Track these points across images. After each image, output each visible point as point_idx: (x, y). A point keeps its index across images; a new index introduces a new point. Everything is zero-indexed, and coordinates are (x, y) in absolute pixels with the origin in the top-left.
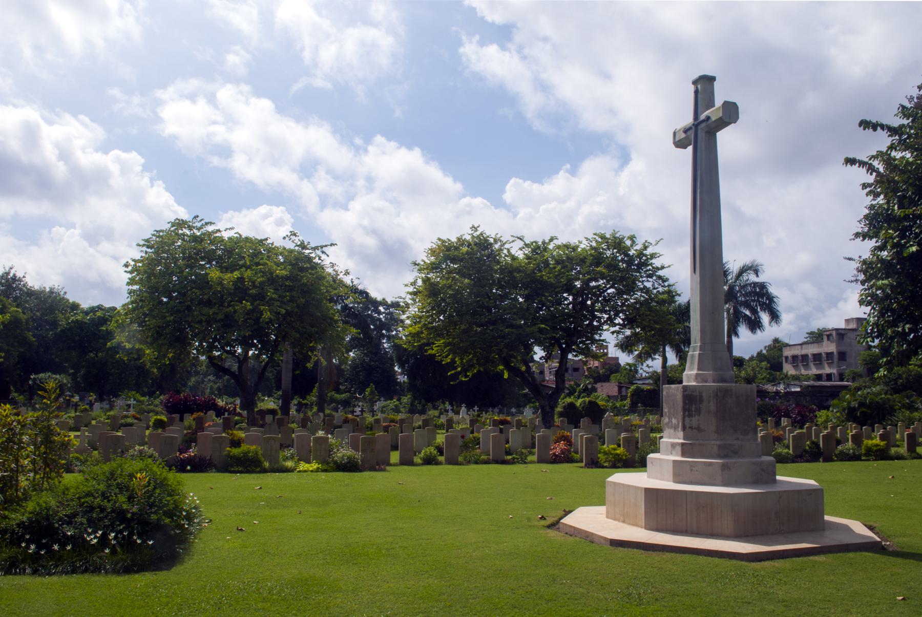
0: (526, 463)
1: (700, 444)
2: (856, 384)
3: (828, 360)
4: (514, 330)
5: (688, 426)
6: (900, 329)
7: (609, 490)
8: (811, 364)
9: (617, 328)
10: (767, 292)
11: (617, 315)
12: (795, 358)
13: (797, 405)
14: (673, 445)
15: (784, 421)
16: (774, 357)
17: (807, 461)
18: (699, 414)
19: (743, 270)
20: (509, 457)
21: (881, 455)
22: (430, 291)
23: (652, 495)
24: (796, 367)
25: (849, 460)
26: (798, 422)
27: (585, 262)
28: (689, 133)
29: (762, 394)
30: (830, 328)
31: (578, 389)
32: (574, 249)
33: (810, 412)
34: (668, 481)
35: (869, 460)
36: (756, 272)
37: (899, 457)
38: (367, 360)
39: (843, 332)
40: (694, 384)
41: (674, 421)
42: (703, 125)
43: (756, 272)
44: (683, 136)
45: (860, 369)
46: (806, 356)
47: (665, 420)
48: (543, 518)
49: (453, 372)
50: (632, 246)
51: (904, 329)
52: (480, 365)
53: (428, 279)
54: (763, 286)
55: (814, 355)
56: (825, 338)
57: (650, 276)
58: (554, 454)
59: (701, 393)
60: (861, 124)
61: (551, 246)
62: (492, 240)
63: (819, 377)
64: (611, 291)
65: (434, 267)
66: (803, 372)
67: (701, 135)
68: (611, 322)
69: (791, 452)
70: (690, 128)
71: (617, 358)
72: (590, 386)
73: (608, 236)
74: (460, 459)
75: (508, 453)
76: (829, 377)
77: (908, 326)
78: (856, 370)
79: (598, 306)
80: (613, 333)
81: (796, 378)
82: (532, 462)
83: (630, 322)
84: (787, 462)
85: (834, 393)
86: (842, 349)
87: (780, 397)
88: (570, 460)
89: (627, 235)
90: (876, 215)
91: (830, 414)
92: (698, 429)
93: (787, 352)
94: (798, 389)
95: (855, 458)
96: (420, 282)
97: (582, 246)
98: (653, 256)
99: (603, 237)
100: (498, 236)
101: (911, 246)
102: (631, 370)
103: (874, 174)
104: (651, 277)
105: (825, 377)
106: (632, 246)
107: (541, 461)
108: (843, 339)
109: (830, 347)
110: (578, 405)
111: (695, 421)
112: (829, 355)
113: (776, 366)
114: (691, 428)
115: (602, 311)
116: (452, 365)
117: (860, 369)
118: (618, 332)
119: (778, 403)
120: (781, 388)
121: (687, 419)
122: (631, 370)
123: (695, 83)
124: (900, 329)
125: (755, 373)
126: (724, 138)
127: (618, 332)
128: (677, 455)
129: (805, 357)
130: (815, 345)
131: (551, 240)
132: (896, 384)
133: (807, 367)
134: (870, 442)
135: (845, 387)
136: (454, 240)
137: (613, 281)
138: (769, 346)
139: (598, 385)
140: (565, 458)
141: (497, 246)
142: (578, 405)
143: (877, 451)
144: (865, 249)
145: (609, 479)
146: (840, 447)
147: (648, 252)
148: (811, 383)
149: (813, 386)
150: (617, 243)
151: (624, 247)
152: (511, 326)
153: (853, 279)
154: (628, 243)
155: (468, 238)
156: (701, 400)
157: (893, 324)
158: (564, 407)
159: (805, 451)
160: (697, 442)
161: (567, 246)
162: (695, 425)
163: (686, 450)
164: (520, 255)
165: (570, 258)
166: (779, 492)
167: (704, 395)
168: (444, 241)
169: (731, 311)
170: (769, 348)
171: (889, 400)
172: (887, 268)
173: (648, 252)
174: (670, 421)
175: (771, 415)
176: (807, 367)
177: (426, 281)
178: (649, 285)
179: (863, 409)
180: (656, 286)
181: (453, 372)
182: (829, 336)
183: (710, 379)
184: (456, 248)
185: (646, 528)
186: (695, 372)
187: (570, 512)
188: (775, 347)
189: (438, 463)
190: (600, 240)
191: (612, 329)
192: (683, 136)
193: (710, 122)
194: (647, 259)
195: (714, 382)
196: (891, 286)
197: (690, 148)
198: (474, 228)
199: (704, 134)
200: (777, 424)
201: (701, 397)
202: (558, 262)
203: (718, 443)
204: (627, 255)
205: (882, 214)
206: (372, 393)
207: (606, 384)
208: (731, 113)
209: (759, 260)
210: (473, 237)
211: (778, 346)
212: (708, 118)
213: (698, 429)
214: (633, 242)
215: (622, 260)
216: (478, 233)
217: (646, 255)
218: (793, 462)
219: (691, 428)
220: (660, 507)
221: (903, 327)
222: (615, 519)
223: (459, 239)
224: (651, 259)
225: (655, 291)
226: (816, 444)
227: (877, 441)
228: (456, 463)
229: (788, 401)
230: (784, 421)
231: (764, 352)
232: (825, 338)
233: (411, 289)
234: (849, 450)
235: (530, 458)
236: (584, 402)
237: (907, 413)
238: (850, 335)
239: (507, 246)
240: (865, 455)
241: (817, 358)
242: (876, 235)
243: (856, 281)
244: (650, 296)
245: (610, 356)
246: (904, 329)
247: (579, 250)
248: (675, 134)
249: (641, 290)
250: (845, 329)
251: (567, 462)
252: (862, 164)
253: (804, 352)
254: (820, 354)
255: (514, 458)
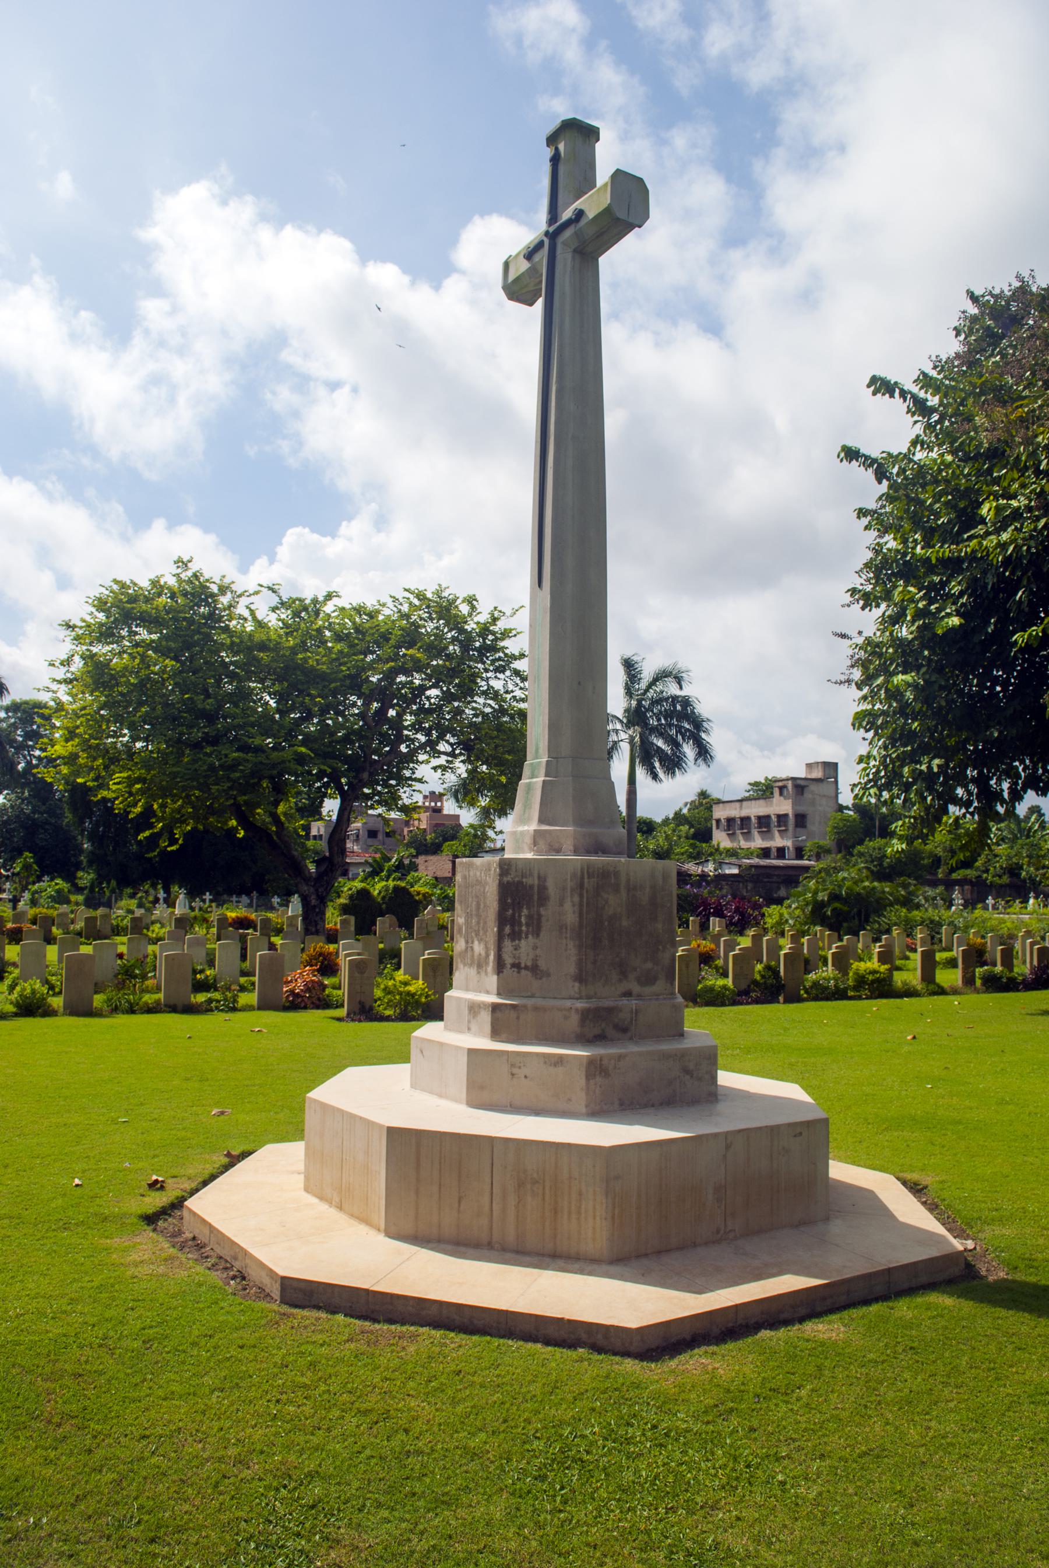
0: (234, 1009)
1: (536, 1009)
2: (821, 865)
3: (779, 826)
4: (250, 756)
5: (508, 960)
6: (924, 767)
7: (311, 1119)
8: (755, 833)
9: (442, 760)
10: (693, 712)
11: (441, 737)
12: (730, 821)
13: (734, 897)
14: (474, 1008)
15: (716, 924)
16: (698, 823)
17: (757, 1001)
18: (537, 933)
19: (661, 676)
20: (201, 998)
21: (881, 988)
22: (99, 676)
23: (408, 1146)
24: (732, 836)
25: (827, 999)
26: (735, 924)
27: (388, 640)
28: (537, 258)
29: (683, 877)
30: (784, 776)
31: (387, 865)
32: (372, 615)
33: (754, 909)
34: (456, 1100)
35: (860, 998)
36: (679, 680)
37: (909, 993)
38: (28, 809)
39: (802, 783)
40: (530, 855)
41: (478, 948)
42: (568, 233)
43: (679, 680)
44: (524, 266)
45: (827, 842)
46: (748, 818)
47: (460, 945)
48: (154, 1185)
49: (147, 833)
50: (470, 615)
51: (930, 768)
52: (197, 819)
53: (93, 656)
54: (686, 702)
55: (759, 818)
56: (776, 791)
57: (501, 670)
58: (292, 992)
59: (542, 879)
60: (874, 380)
61: (329, 608)
62: (214, 589)
63: (766, 853)
64: (434, 692)
65: (106, 634)
66: (744, 844)
67: (565, 258)
68: (431, 746)
69: (729, 982)
70: (539, 245)
71: (458, 817)
72: (407, 862)
73: (429, 595)
74: (98, 1000)
75: (201, 986)
76: (781, 852)
77: (936, 762)
78: (822, 843)
79: (409, 719)
80: (435, 768)
81: (734, 852)
82: (248, 1008)
83: (469, 748)
84: (723, 1005)
85: (791, 878)
86: (802, 809)
87: (708, 883)
88: (324, 1004)
89: (462, 595)
90: (886, 563)
91: (785, 911)
92: (534, 969)
93: (720, 813)
94: (736, 871)
95: (839, 994)
96: (78, 664)
97: (387, 612)
98: (506, 634)
99: (421, 596)
100: (227, 581)
101: (949, 615)
102: (475, 836)
103: (885, 483)
104: (503, 672)
105: (774, 853)
106: (470, 615)
107: (264, 1005)
108: (802, 794)
109: (782, 806)
110: (376, 893)
111: (526, 949)
112: (782, 818)
113: (704, 835)
114: (516, 966)
115: (417, 727)
116: (146, 818)
117: (827, 842)
118: (444, 768)
119: (705, 892)
120: (710, 868)
121: (508, 944)
122: (475, 836)
123: (552, 140)
124: (924, 767)
125: (670, 844)
126: (616, 263)
127: (444, 768)
128: (480, 1034)
129: (745, 821)
130: (762, 802)
131: (329, 597)
132: (881, 865)
133: (748, 836)
134: (863, 966)
135: (806, 869)
136: (145, 584)
137: (438, 677)
138: (693, 802)
139: (420, 860)
140: (313, 999)
141: (225, 600)
142: (376, 893)
143: (873, 982)
144: (868, 622)
145: (314, 1094)
146: (812, 976)
147: (501, 625)
148: (755, 861)
149: (757, 867)
150: (444, 609)
151: (456, 616)
152: (245, 748)
153: (843, 678)
154: (464, 609)
155: (172, 582)
156: (543, 898)
157: (912, 758)
158: (351, 897)
159: (755, 982)
160: (530, 1002)
161: (359, 610)
162: (526, 960)
163: (503, 1022)
164: (273, 620)
165: (365, 633)
166: (727, 1134)
167: (550, 884)
168: (123, 585)
169: (637, 739)
170: (694, 806)
171: (874, 888)
172: (907, 655)
173: (501, 625)
174: (469, 948)
175: (693, 912)
176: (748, 836)
177: (89, 658)
178: (497, 685)
179: (837, 905)
180: (511, 687)
181: (147, 833)
182: (781, 789)
183: (568, 844)
184: (147, 600)
185: (389, 1234)
186: (533, 826)
187: (245, 1155)
188: (701, 804)
189: (49, 1012)
190: (416, 602)
191: (435, 762)
192: (524, 266)
193: (583, 222)
194: (496, 639)
195: (576, 852)
196: (915, 686)
197: (540, 303)
198: (182, 563)
199: (569, 256)
200: (704, 927)
201: (542, 888)
202: (338, 637)
203: (580, 1005)
204: (462, 631)
205: (897, 561)
206: (26, 867)
207: (432, 858)
208: (630, 205)
209: (682, 665)
210: (180, 581)
211: (705, 801)
212: (580, 214)
213: (534, 969)
214: (473, 608)
215: (454, 639)
216: (189, 573)
217: (494, 633)
218: (734, 1003)
219: (516, 966)
220: (431, 1182)
221: (929, 762)
222: (322, 1198)
223: (155, 583)
224: (503, 639)
225: (509, 696)
226: (772, 970)
227: (873, 964)
228: (90, 1012)
229: (721, 889)
230: (716, 924)
231: (685, 811)
232: (776, 791)
233: (61, 673)
234: (828, 980)
235: (244, 999)
236: (386, 888)
237: (904, 911)
238: (813, 787)
239: (244, 601)
240: (856, 988)
241: (764, 822)
242: (887, 596)
243: (849, 681)
244: (500, 706)
245: (445, 812)
246: (930, 768)
247: (381, 617)
248: (506, 265)
249: (485, 693)
250: (805, 779)
251: (318, 1007)
252: (868, 462)
253: (744, 813)
254: (768, 817)
255: (210, 1001)
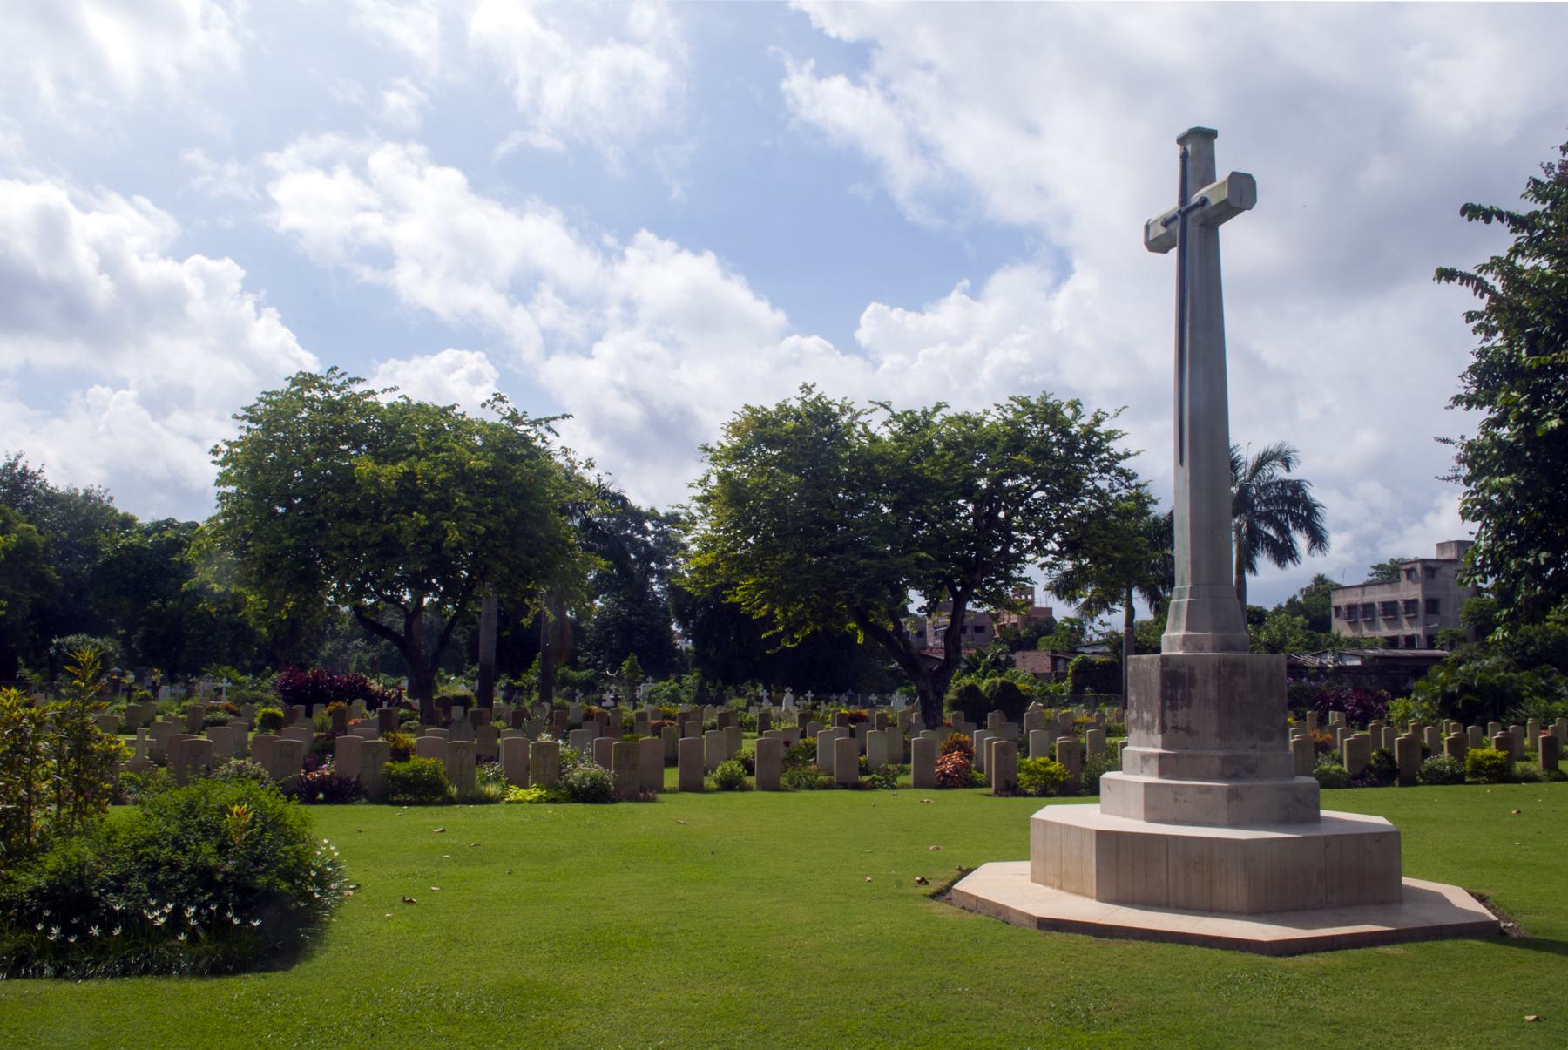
0: (894, 788)
1: (1190, 756)
2: (1456, 654)
3: (1407, 612)
4: (874, 562)
5: (1169, 725)
6: (1530, 560)
7: (1035, 834)
8: (1380, 620)
9: (1049, 558)
10: (1305, 496)
11: (1049, 536)
12: (1351, 609)
13: (1355, 690)
14: (1145, 758)
15: (1334, 717)
16: (1316, 607)
17: (1373, 785)
18: (1189, 705)
19: (1264, 460)
20: (866, 778)
21: (1499, 774)
22: (732, 496)
23: (1108, 842)
24: (1354, 625)
25: (1443, 783)
26: (1357, 718)
27: (995, 447)
28: (1172, 226)
29: (1296, 670)
30: (1412, 558)
31: (983, 662)
32: (977, 423)
33: (1377, 702)
34: (1136, 818)
35: (1477, 783)
36: (1286, 463)
37: (1529, 778)
38: (624, 612)
39: (1433, 565)
40: (1180, 653)
41: (1146, 716)
42: (1196, 213)
43: (1286, 463)
44: (1162, 231)
45: (1462, 628)
46: (1371, 605)
47: (1132, 715)
48: (923, 881)
49: (770, 633)
50: (1074, 418)
51: (1537, 560)
52: (817, 621)
53: (729, 475)
54: (1297, 487)
55: (1384, 604)
56: (1403, 575)
57: (1106, 470)
58: (943, 772)
59: (1191, 669)
60: (1464, 211)
61: (937, 419)
62: (836, 409)
63: (1392, 642)
64: (1039, 495)
65: (738, 455)
66: (1366, 633)
67: (1193, 229)
68: (1039, 547)
69: (1345, 769)
70: (1174, 219)
71: (1050, 610)
72: (1003, 658)
73: (1034, 401)
74: (783, 781)
75: (864, 770)
76: (1410, 642)
77: (1544, 555)
78: (1455, 630)
79: (1017, 520)
80: (1042, 566)
81: (1354, 643)
82: (905, 787)
83: (1071, 547)
84: (1338, 787)
85: (1419, 668)
86: (1433, 593)
87: (1327, 676)
88: (970, 783)
89: (1066, 399)
90: (1491, 365)
91: (1411, 705)
92: (1188, 730)
93: (1339, 600)
94: (1358, 663)
95: (1455, 779)
96: (714, 481)
97: (990, 419)
98: (1110, 436)
99: (1025, 403)
100: (847, 402)
101: (1550, 418)
102: (1072, 630)
103: (1487, 296)
104: (1108, 472)
105: (1402, 642)
106: (1074, 418)
107: (919, 784)
108: (1433, 576)
109: (1411, 591)
110: (983, 689)
111: (1181, 716)
112: (1410, 605)
113: (1320, 623)
114: (1175, 728)
115: (1024, 529)
116: (768, 621)
117: (1462, 628)
118: (1051, 566)
119: (1323, 685)
120: (1328, 660)
121: (1168, 713)
122: (1072, 630)
123: (1182, 140)
124: (1530, 560)
125: (1284, 635)
126: (1232, 234)
127: (1051, 566)
128: (1151, 774)
129: (1368, 608)
130: (1387, 587)
131: (938, 408)
132: (1524, 653)
133: (1372, 624)
134: (1479, 753)
135: (1438, 659)
136: (772, 408)
137: (1042, 478)
138: (1308, 589)
139: (1017, 656)
140: (961, 780)
141: (845, 419)
142: (983, 689)
143: (1491, 767)
144: (1472, 423)
145: (1035, 816)
146: (1428, 761)
147: (1103, 428)
148: (1380, 651)
149: (1382, 658)
150: (1050, 414)
151: (1062, 421)
152: (870, 555)
153: (1451, 474)
154: (1069, 413)
155: (796, 404)
156: (1192, 680)
157: (1520, 552)
158: (960, 693)
159: (1370, 767)
160: (1185, 752)
161: (964, 419)
162: (1181, 723)
163: (1166, 766)
164: (885, 434)
165: (970, 439)
166: (1325, 837)
167: (1197, 672)
168: (754, 411)
169: (1244, 529)
170: (1309, 593)
171: (1511, 680)
172: (1508, 456)
173: (1103, 428)
174: (1140, 717)
175: (1311, 706)
176: (1372, 624)
177: (724, 477)
178: (1103, 485)
179: (1468, 697)
180: (1116, 486)
181: (770, 633)
182: (1409, 572)
183: (1208, 645)
184: (776, 423)
185: (1099, 899)
186: (1182, 633)
187: (970, 871)
188: (1318, 591)
189: (745, 788)
190: (1020, 408)
191: (1041, 560)
192: (1162, 231)
193: (1207, 207)
194: (1101, 441)
195: (1214, 650)
196: (1515, 486)
197: (1174, 252)
198: (807, 389)
199: (1197, 229)
200: (1322, 721)
201: (1192, 675)
202: (948, 446)
203: (1221, 753)
204: (1066, 434)
205: (1500, 365)
206: (632, 669)
207: (1030, 654)
208: (1242, 193)
209: (1291, 443)
210: (804, 403)
211: (1322, 588)
212: (1204, 201)
213: (1188, 730)
214: (1077, 412)
215: (1059, 442)
216: (813, 396)
217: (1098, 435)
218: (1349, 786)
219: (1175, 728)
220: (1122, 863)
221: (1536, 557)
222: (1045, 884)
223: (780, 407)
224: (1108, 440)
225: (1114, 496)
226: (1388, 756)
227: (1491, 750)
228: (776, 788)
229: (1341, 682)
230: (1334, 717)
231: (1300, 599)
232: (1403, 575)
233: (699, 492)
234: (1444, 765)
235: (901, 780)
236: (994, 683)
237: (1543, 703)
238: (1446, 570)
239: (862, 419)
240: (1472, 774)
241: (1390, 609)
242: (1490, 400)
243: (1456, 477)
244: (1105, 504)
245: (1037, 605)
246: (1537, 560)
247: (985, 425)
248: (1147, 227)
249: (1091, 493)
250: (1436, 561)
251: (965, 786)
252: (1466, 278)
253: (1367, 599)
254: (1395, 603)
255: (874, 780)
